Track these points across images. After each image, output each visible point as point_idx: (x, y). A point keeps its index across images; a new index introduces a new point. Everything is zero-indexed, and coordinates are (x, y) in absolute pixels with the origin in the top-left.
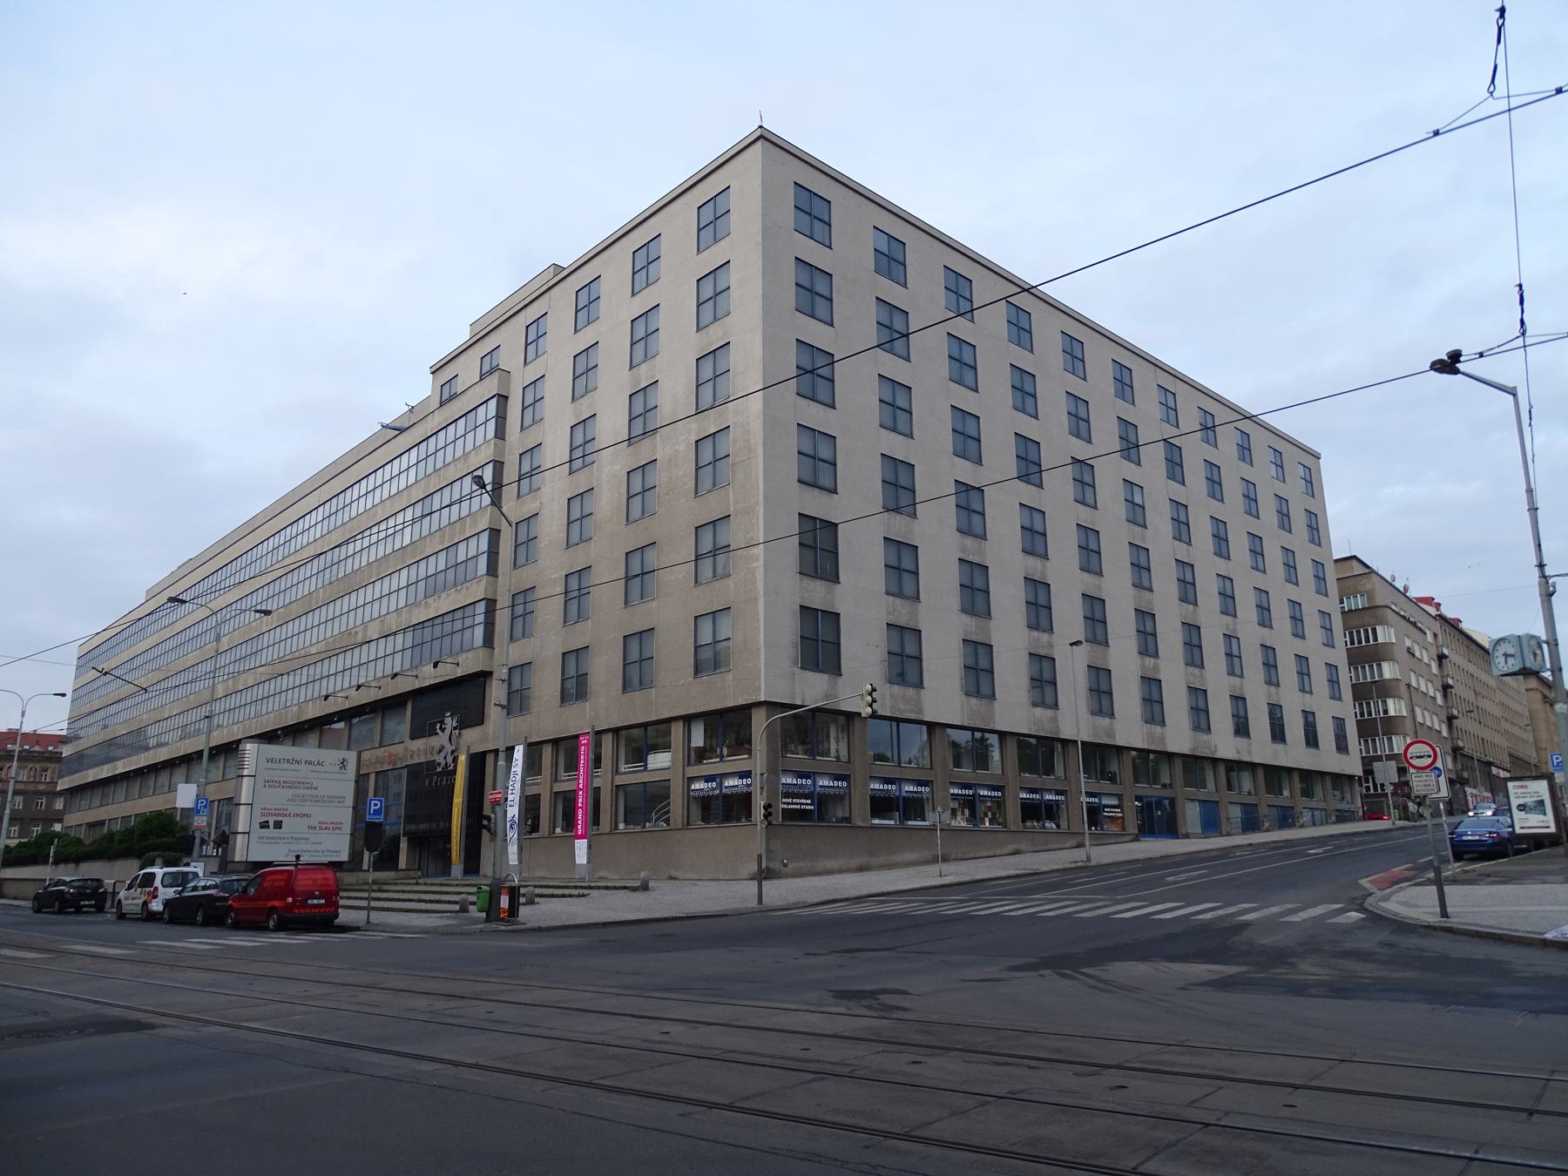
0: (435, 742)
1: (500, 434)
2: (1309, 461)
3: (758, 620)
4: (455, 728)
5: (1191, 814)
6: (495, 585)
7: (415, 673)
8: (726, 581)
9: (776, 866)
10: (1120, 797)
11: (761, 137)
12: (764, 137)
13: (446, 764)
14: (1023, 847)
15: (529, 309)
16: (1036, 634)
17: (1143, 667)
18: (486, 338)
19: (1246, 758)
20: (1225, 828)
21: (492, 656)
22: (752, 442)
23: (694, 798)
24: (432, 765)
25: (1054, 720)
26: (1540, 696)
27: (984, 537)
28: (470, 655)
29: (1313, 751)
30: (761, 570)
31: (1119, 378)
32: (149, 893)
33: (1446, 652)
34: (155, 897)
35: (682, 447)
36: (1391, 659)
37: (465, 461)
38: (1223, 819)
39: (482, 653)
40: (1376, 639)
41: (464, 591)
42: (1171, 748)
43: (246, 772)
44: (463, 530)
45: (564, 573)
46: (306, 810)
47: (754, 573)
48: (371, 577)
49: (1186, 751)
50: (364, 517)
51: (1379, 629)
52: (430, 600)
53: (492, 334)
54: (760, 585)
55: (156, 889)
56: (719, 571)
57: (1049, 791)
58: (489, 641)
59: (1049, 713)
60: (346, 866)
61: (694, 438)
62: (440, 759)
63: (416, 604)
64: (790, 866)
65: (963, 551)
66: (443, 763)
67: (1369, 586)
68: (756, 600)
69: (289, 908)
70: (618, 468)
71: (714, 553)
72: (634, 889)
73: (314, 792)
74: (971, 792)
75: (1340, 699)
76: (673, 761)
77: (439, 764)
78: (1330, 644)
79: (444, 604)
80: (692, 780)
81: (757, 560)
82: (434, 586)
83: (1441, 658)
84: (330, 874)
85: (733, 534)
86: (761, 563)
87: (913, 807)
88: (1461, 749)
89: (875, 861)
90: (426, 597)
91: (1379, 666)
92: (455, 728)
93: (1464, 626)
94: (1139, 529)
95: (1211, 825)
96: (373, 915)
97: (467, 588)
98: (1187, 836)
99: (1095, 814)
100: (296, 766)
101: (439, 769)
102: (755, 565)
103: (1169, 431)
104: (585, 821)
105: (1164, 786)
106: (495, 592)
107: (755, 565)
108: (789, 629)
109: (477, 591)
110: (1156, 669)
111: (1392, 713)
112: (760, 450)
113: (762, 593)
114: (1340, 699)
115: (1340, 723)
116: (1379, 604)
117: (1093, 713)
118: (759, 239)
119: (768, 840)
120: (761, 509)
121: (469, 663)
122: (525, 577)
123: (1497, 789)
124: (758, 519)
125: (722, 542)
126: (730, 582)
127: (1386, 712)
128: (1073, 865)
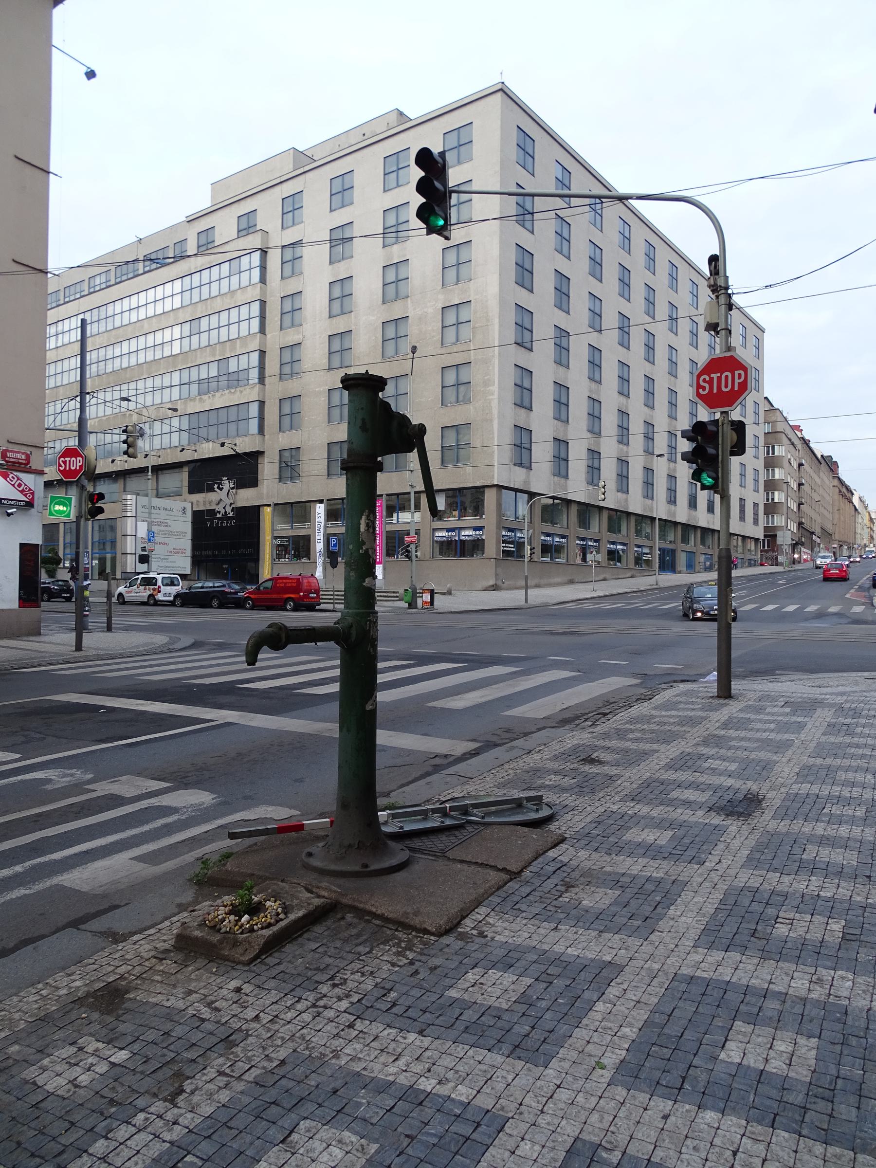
0: (213, 496)
1: (263, 280)
2: (758, 333)
3: (493, 433)
4: (232, 488)
5: (682, 559)
6: (264, 390)
7: (194, 448)
8: (467, 406)
9: (499, 583)
10: (651, 548)
11: (501, 90)
12: (503, 90)
13: (226, 512)
14: (607, 576)
15: (285, 185)
16: (621, 446)
17: (669, 468)
18: (242, 202)
19: (711, 527)
20: (697, 569)
21: (264, 440)
22: (490, 314)
23: (437, 542)
24: (212, 512)
25: (626, 500)
26: (837, 490)
27: (600, 382)
28: (247, 439)
29: (742, 523)
30: (496, 401)
31: (560, 232)
32: (154, 590)
33: (803, 462)
34: (160, 592)
35: (430, 310)
36: (780, 466)
37: (232, 297)
38: (697, 563)
39: (258, 437)
40: (773, 453)
41: (238, 393)
42: (678, 520)
43: (129, 514)
44: (233, 348)
45: (327, 388)
46: (166, 540)
47: (490, 403)
48: (142, 374)
49: (684, 521)
50: (130, 328)
51: (776, 448)
52: (205, 397)
53: (249, 200)
54: (495, 411)
55: (159, 587)
56: (461, 398)
57: (591, 539)
58: (261, 430)
59: (624, 496)
60: (189, 577)
61: (440, 306)
62: (219, 508)
63: (189, 398)
64: (506, 583)
65: (590, 391)
66: (223, 511)
67: (773, 419)
68: (491, 420)
69: (302, 598)
70: (372, 318)
71: (458, 385)
72: (444, 594)
73: (168, 529)
74: (584, 543)
75: (758, 492)
76: (422, 518)
77: (219, 512)
78: (756, 457)
79: (220, 400)
80: (434, 530)
81: (493, 394)
82: (206, 386)
83: (801, 465)
84: (543, 582)
85: (475, 375)
86: (496, 396)
87: (559, 549)
88: (803, 523)
89: (543, 582)
90: (199, 394)
91: (773, 470)
92: (232, 488)
93: (811, 445)
94: (673, 378)
95: (691, 567)
96: (336, 606)
97: (241, 392)
98: (680, 572)
99: (638, 560)
100: (158, 511)
101: (218, 515)
102: (491, 397)
103: (694, 312)
104: (381, 554)
105: (670, 542)
106: (264, 396)
107: (491, 397)
108: (509, 438)
109: (251, 393)
110: (675, 470)
111: (776, 500)
112: (496, 321)
113: (496, 416)
114: (758, 492)
115: (756, 505)
116: (778, 430)
117: (644, 497)
118: (498, 168)
119: (496, 567)
120: (496, 361)
121: (244, 445)
122: (292, 387)
123: (812, 546)
124: (494, 367)
125: (464, 379)
126: (471, 407)
127: (773, 499)
128: (649, 587)
